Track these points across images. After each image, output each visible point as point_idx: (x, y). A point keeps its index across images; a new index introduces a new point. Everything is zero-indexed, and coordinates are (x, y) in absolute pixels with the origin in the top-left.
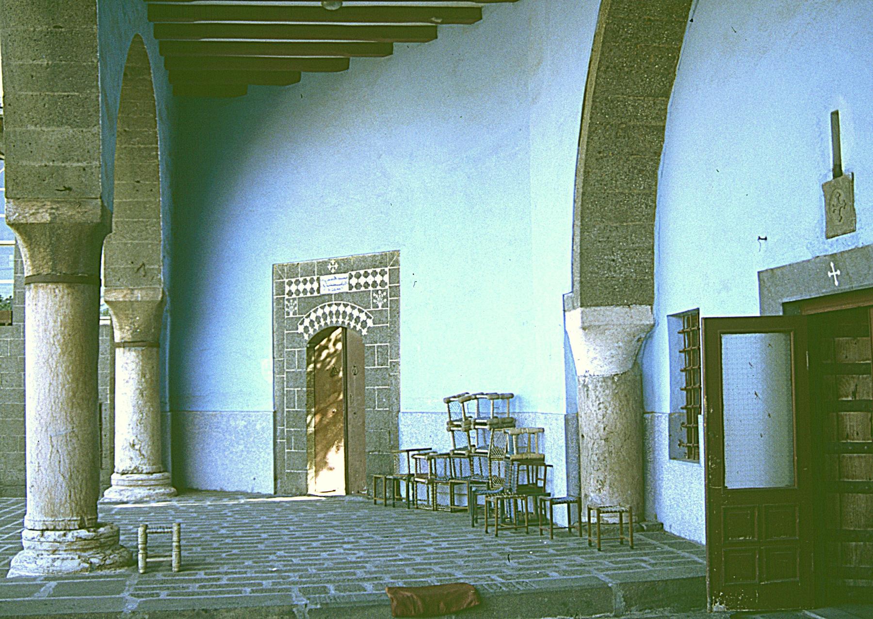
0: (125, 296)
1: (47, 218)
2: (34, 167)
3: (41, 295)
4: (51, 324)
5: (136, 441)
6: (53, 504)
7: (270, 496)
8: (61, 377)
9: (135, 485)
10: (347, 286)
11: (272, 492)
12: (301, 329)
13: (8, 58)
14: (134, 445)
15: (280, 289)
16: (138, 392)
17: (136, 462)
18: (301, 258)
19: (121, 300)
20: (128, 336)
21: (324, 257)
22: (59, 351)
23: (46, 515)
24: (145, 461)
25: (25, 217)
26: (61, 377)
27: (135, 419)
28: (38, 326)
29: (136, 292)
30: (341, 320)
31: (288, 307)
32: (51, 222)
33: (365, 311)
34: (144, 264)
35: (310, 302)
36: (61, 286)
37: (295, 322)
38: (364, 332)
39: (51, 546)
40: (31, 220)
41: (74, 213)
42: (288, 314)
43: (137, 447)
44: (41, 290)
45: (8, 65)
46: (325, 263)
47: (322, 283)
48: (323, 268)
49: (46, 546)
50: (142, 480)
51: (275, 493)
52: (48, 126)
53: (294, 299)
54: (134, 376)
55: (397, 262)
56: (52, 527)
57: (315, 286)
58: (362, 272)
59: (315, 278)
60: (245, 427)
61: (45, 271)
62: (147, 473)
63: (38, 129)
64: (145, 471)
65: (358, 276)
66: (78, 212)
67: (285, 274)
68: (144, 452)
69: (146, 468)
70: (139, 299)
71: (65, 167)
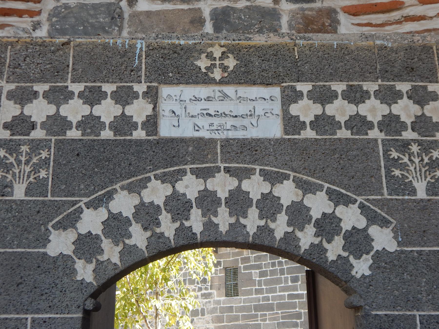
37: (34, 221)
47: (165, 107)
53: (37, 146)
59: (140, 88)
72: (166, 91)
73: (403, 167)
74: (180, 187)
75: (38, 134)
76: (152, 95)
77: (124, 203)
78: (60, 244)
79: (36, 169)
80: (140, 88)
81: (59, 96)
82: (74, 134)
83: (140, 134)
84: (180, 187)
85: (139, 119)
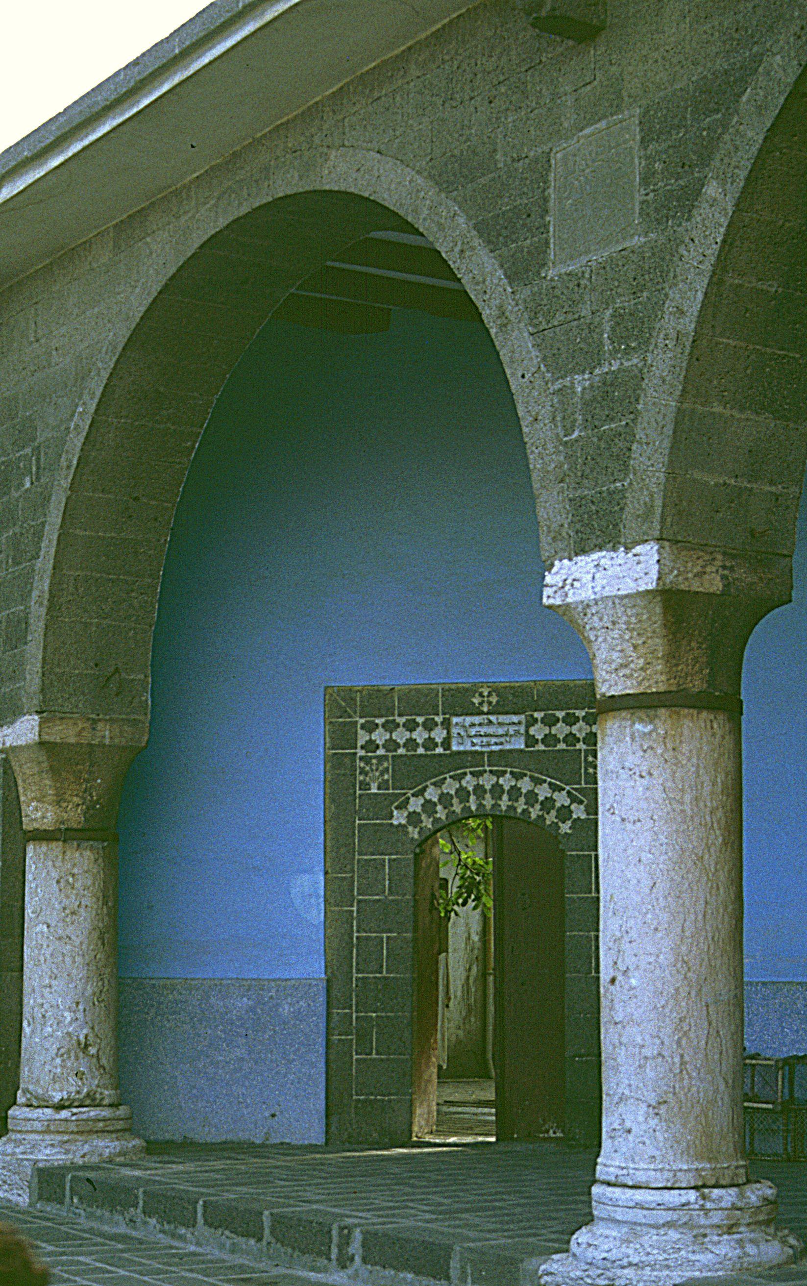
0: (79, 734)
1: (717, 586)
2: (706, 484)
3: (686, 732)
4: (707, 789)
5: (91, 1039)
6: (709, 1136)
7: (313, 1148)
8: (722, 890)
9: (87, 1130)
10: (522, 740)
11: (321, 1141)
12: (399, 818)
13: (725, 270)
14: (86, 1046)
15: (342, 737)
16: (96, 935)
17: (92, 1083)
18: (399, 675)
19: (72, 740)
20: (75, 816)
21: (463, 680)
22: (720, 839)
23: (699, 1157)
24: (106, 1080)
25: (687, 579)
26: (722, 890)
27: (89, 990)
28: (682, 790)
29: (100, 726)
30: (488, 802)
31: (363, 772)
32: (723, 594)
33: (568, 788)
34: (117, 670)
35: (416, 770)
36: (721, 717)
37: (381, 806)
38: (565, 828)
39: (728, 1217)
40: (696, 587)
41: (755, 579)
42: (365, 786)
43: (92, 1050)
44: (687, 722)
45: (721, 282)
46: (473, 690)
47: (454, 731)
48: (459, 702)
49: (716, 1218)
50: (104, 1120)
51: (327, 1143)
52: (742, 410)
53: (381, 759)
54: (88, 901)
55: (349, 694)
56: (713, 1182)
57: (439, 735)
58: (560, 714)
59: (439, 719)
60: (252, 1010)
61: (697, 685)
62: (110, 1105)
63: (728, 412)
64: (106, 1102)
65: (550, 721)
66: (761, 579)
67: (349, 709)
68: (104, 1062)
69: (108, 1095)
70: (107, 741)
71: (751, 490)
72: (455, 720)
73: (366, 774)
74: (464, 783)
75: (381, 752)
76: (447, 724)
77: (432, 794)
78: (399, 818)
79: (382, 774)
80: (439, 719)
81: (391, 726)
82: (401, 751)
83: (439, 750)
84: (464, 783)
85: (439, 740)
